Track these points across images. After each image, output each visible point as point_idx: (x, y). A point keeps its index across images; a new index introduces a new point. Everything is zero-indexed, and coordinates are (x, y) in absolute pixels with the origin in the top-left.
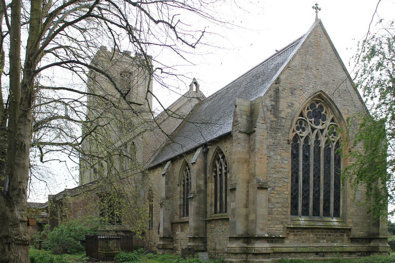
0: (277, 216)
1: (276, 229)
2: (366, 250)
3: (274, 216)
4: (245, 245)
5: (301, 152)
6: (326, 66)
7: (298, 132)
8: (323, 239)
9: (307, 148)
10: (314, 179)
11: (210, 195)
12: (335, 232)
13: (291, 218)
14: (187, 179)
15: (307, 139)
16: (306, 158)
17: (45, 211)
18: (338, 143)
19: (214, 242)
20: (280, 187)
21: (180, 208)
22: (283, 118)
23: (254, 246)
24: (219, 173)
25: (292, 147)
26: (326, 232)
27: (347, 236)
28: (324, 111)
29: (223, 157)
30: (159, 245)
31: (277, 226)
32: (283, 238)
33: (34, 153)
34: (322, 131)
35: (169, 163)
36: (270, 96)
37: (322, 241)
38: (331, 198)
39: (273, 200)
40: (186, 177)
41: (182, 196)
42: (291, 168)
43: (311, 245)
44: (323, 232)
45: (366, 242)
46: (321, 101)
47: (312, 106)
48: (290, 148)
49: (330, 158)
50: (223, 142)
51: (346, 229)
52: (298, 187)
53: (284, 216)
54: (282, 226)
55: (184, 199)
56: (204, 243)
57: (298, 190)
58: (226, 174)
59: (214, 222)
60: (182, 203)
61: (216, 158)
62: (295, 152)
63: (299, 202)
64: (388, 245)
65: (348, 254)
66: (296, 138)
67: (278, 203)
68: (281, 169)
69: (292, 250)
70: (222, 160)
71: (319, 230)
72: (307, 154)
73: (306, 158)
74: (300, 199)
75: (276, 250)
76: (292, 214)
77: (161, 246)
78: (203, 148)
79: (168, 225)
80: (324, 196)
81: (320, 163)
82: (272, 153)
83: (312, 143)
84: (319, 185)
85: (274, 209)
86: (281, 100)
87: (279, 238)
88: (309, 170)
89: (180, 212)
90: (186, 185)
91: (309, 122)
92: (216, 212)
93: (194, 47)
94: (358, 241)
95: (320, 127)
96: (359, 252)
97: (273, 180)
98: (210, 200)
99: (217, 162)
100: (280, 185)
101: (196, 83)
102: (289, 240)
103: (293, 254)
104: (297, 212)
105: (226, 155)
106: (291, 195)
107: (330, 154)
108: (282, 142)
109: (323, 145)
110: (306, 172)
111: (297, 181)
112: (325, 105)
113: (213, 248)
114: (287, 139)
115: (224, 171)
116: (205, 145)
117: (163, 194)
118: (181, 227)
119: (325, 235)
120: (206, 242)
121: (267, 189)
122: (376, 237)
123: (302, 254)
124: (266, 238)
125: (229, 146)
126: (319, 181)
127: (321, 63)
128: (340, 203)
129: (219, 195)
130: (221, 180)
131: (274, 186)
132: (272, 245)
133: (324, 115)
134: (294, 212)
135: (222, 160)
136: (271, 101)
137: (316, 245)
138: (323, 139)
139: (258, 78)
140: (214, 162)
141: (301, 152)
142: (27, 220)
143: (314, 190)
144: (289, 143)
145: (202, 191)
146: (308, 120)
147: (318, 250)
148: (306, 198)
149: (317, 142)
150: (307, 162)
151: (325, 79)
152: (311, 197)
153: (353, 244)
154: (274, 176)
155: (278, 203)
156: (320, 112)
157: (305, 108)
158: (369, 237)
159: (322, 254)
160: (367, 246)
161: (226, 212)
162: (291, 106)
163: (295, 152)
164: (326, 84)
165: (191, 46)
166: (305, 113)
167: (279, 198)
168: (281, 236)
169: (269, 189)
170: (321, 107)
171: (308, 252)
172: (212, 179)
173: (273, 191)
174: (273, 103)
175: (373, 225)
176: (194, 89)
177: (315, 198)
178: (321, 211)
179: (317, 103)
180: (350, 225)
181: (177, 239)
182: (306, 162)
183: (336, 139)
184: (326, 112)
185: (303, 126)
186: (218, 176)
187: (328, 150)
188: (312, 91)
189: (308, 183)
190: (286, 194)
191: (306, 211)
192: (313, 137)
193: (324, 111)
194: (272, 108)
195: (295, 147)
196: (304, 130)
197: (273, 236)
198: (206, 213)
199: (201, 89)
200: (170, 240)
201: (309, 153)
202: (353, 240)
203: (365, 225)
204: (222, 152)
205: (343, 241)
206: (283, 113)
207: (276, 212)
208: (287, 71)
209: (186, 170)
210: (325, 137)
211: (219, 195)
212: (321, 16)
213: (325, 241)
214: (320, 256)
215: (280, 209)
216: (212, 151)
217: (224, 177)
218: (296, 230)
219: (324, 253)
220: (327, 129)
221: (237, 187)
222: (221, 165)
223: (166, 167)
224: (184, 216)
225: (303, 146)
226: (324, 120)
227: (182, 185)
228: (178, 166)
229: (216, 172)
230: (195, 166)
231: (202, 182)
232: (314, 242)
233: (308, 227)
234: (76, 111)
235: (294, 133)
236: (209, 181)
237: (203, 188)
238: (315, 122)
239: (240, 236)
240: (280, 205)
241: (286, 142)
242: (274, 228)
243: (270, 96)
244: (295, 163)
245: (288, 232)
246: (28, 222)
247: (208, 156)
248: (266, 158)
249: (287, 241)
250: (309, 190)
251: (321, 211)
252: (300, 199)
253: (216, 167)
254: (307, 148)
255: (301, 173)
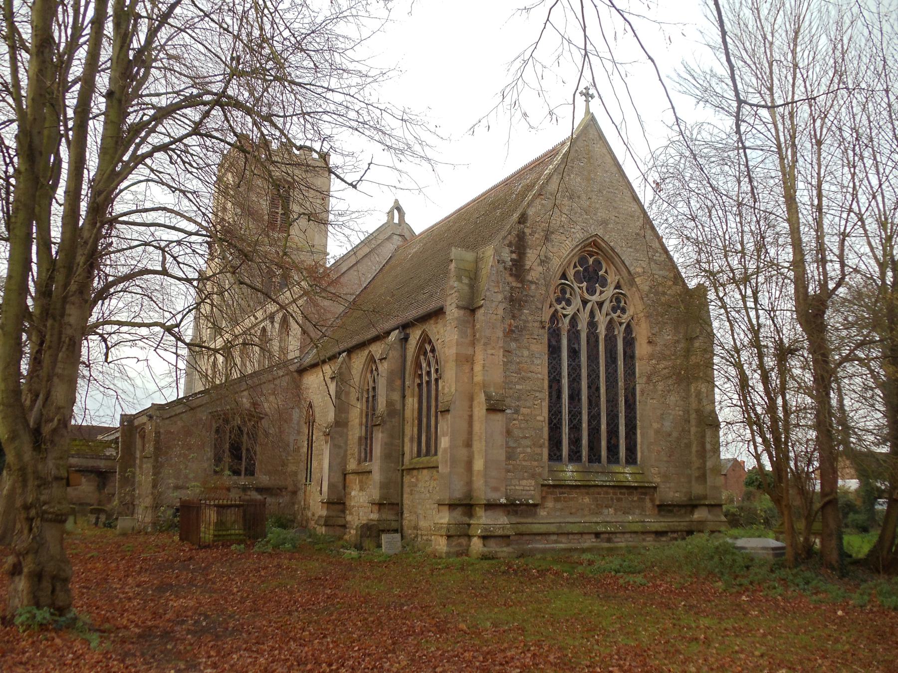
0: (524, 463)
1: (522, 488)
2: (685, 529)
3: (518, 462)
4: (466, 519)
5: (565, 342)
6: (605, 192)
7: (559, 307)
8: (607, 507)
9: (574, 335)
10: (589, 393)
11: (410, 421)
12: (630, 494)
13: (549, 466)
14: (374, 388)
15: (574, 320)
16: (574, 353)
17: (113, 445)
18: (628, 326)
19: (415, 513)
20: (529, 408)
21: (360, 444)
22: (531, 282)
23: (23, 578)
24: (425, 378)
25: (549, 334)
26: (615, 494)
27: (652, 500)
28: (604, 270)
29: (433, 350)
30: (320, 517)
31: (524, 482)
32: (535, 505)
33: (91, 348)
34: (600, 304)
35: (344, 354)
36: (510, 245)
37: (605, 511)
38: (620, 428)
39: (516, 432)
40: (371, 383)
41: (364, 420)
42: (547, 371)
43: (587, 519)
44: (607, 493)
45: (686, 513)
46: (597, 253)
47: (582, 261)
48: (546, 336)
49: (616, 353)
50: (432, 322)
51: (648, 487)
52: (561, 407)
53: (536, 463)
54: (533, 483)
55: (366, 427)
56: (397, 514)
57: (560, 412)
58: (437, 380)
59: (415, 472)
60: (363, 434)
61: (421, 351)
62: (554, 343)
63: (564, 436)
64: (723, 518)
65: (653, 536)
66: (554, 317)
67: (526, 438)
68: (530, 375)
69: (553, 528)
70: (430, 355)
71: (599, 490)
72: (576, 346)
73: (574, 353)
74: (565, 430)
75: (523, 528)
76: (551, 458)
77: (323, 519)
78: (400, 332)
79: (338, 478)
80: (608, 424)
81: (598, 363)
82: (513, 345)
83: (582, 326)
84: (598, 405)
85: (518, 450)
86: (528, 251)
87: (528, 505)
88: (579, 376)
89: (360, 453)
90: (370, 399)
91: (577, 289)
92: (419, 454)
93: (355, 187)
94: (670, 511)
95: (595, 298)
96: (673, 532)
97: (516, 395)
98: (410, 430)
99: (422, 357)
100: (528, 404)
101: (400, 209)
102: (547, 510)
103: (554, 538)
104: (561, 455)
105: (438, 346)
106: (550, 423)
107: (616, 346)
108: (530, 325)
109: (602, 330)
110: (574, 379)
111: (559, 397)
112: (604, 259)
113: (413, 523)
114: (539, 319)
115: (434, 376)
116: (405, 326)
117: (331, 417)
118: (361, 482)
119: (612, 499)
120: (402, 513)
121: (503, 411)
122: (702, 502)
123: (571, 537)
124: (501, 505)
125: (442, 331)
126: (599, 396)
127: (596, 187)
128: (636, 438)
129: (424, 420)
130: (429, 391)
131: (518, 406)
132: (514, 520)
133: (603, 276)
134: (555, 455)
135: (430, 355)
136: (512, 252)
137: (595, 520)
138: (602, 320)
139: (495, 208)
140: (418, 357)
141: (565, 342)
142: (66, 475)
143: (589, 413)
144: (544, 327)
145: (395, 412)
146: (575, 286)
147: (600, 529)
148: (575, 428)
149: (592, 325)
150: (577, 360)
151: (602, 214)
152: (585, 425)
153: (663, 516)
154: (518, 387)
155: (526, 438)
156: (596, 272)
157: (569, 264)
158: (690, 503)
159: (607, 536)
160: (688, 519)
161: (436, 454)
162: (544, 261)
163: (554, 343)
164: (604, 223)
165: (351, 184)
166: (571, 273)
167: (527, 429)
168: (531, 502)
169: (508, 411)
170: (598, 263)
171: (582, 534)
172: (413, 389)
173: (515, 416)
174: (514, 256)
175: (698, 478)
176: (396, 220)
177: (593, 429)
178: (604, 453)
179: (591, 256)
180: (655, 480)
181: (354, 507)
182: (574, 360)
183: (625, 318)
184: (606, 272)
185: (568, 296)
186: (424, 385)
187: (611, 339)
188: (579, 236)
189: (580, 400)
190: (539, 421)
191: (576, 453)
192: (584, 318)
193: (604, 270)
194: (513, 265)
195: (555, 334)
196: (569, 303)
197: (518, 502)
198: (403, 455)
199: (408, 219)
200: (341, 507)
201: (579, 344)
202: (664, 508)
203: (682, 480)
204: (430, 342)
205: (643, 509)
206: (533, 273)
207: (522, 455)
208: (538, 201)
209: (372, 371)
210: (607, 315)
211: (424, 420)
212: (595, 106)
213: (611, 510)
214: (602, 541)
215: (529, 450)
216: (415, 335)
217: (433, 387)
218: (558, 488)
219: (610, 536)
220: (608, 301)
221: (452, 408)
222: (429, 365)
223: (341, 359)
224: (365, 460)
225: (569, 331)
226: (604, 284)
227: (364, 400)
228: (359, 361)
229: (420, 376)
230: (386, 364)
231: (396, 396)
232: (592, 514)
233: (579, 483)
234: (178, 263)
235: (553, 309)
236: (408, 393)
237: (398, 406)
238: (587, 290)
239: (458, 502)
240: (528, 442)
241: (536, 324)
242: (519, 485)
243: (510, 245)
244: (554, 362)
245: (544, 494)
246: (68, 479)
247: (408, 346)
248: (501, 354)
249: (543, 513)
250: (580, 413)
251: (604, 453)
252: (565, 430)
253: (421, 368)
254: (574, 335)
255: (565, 382)
